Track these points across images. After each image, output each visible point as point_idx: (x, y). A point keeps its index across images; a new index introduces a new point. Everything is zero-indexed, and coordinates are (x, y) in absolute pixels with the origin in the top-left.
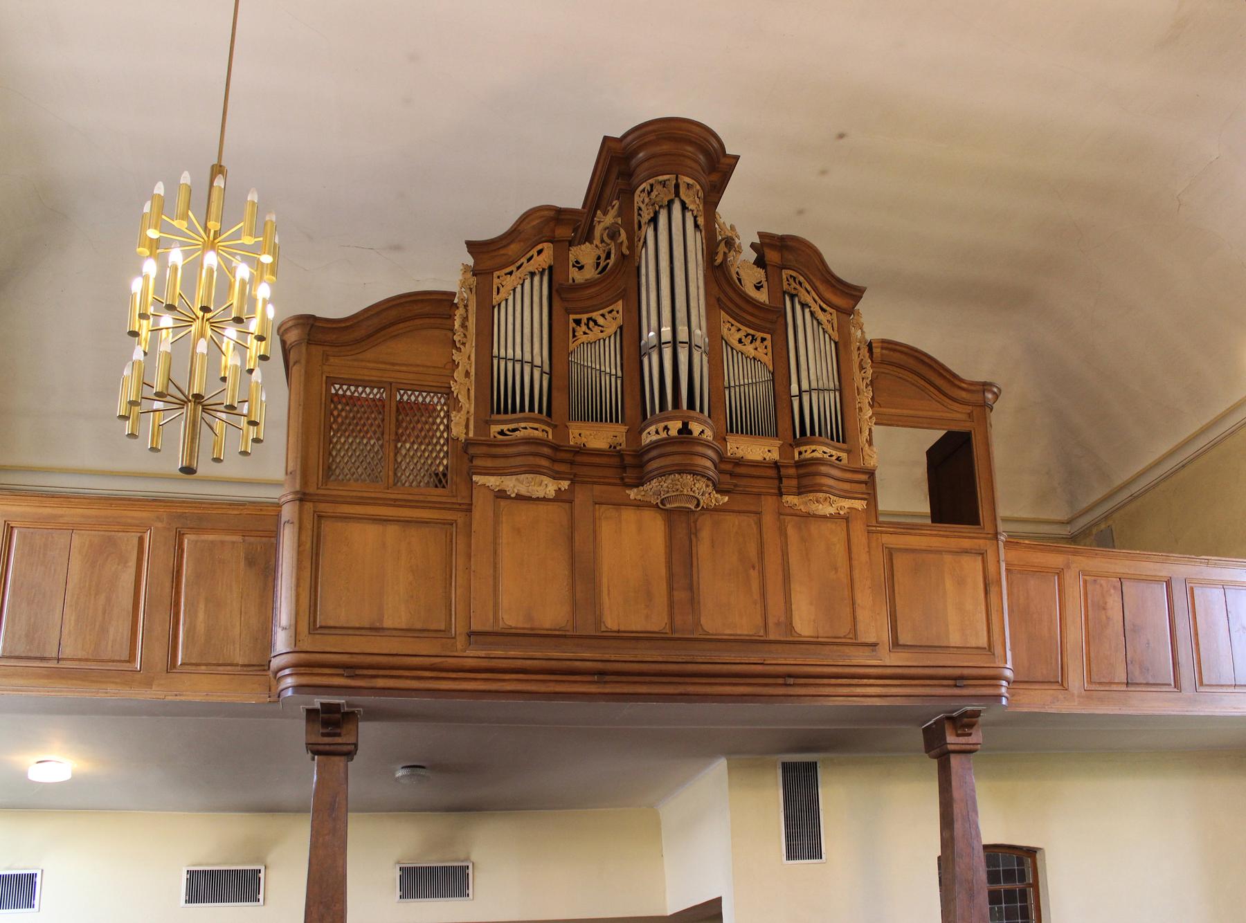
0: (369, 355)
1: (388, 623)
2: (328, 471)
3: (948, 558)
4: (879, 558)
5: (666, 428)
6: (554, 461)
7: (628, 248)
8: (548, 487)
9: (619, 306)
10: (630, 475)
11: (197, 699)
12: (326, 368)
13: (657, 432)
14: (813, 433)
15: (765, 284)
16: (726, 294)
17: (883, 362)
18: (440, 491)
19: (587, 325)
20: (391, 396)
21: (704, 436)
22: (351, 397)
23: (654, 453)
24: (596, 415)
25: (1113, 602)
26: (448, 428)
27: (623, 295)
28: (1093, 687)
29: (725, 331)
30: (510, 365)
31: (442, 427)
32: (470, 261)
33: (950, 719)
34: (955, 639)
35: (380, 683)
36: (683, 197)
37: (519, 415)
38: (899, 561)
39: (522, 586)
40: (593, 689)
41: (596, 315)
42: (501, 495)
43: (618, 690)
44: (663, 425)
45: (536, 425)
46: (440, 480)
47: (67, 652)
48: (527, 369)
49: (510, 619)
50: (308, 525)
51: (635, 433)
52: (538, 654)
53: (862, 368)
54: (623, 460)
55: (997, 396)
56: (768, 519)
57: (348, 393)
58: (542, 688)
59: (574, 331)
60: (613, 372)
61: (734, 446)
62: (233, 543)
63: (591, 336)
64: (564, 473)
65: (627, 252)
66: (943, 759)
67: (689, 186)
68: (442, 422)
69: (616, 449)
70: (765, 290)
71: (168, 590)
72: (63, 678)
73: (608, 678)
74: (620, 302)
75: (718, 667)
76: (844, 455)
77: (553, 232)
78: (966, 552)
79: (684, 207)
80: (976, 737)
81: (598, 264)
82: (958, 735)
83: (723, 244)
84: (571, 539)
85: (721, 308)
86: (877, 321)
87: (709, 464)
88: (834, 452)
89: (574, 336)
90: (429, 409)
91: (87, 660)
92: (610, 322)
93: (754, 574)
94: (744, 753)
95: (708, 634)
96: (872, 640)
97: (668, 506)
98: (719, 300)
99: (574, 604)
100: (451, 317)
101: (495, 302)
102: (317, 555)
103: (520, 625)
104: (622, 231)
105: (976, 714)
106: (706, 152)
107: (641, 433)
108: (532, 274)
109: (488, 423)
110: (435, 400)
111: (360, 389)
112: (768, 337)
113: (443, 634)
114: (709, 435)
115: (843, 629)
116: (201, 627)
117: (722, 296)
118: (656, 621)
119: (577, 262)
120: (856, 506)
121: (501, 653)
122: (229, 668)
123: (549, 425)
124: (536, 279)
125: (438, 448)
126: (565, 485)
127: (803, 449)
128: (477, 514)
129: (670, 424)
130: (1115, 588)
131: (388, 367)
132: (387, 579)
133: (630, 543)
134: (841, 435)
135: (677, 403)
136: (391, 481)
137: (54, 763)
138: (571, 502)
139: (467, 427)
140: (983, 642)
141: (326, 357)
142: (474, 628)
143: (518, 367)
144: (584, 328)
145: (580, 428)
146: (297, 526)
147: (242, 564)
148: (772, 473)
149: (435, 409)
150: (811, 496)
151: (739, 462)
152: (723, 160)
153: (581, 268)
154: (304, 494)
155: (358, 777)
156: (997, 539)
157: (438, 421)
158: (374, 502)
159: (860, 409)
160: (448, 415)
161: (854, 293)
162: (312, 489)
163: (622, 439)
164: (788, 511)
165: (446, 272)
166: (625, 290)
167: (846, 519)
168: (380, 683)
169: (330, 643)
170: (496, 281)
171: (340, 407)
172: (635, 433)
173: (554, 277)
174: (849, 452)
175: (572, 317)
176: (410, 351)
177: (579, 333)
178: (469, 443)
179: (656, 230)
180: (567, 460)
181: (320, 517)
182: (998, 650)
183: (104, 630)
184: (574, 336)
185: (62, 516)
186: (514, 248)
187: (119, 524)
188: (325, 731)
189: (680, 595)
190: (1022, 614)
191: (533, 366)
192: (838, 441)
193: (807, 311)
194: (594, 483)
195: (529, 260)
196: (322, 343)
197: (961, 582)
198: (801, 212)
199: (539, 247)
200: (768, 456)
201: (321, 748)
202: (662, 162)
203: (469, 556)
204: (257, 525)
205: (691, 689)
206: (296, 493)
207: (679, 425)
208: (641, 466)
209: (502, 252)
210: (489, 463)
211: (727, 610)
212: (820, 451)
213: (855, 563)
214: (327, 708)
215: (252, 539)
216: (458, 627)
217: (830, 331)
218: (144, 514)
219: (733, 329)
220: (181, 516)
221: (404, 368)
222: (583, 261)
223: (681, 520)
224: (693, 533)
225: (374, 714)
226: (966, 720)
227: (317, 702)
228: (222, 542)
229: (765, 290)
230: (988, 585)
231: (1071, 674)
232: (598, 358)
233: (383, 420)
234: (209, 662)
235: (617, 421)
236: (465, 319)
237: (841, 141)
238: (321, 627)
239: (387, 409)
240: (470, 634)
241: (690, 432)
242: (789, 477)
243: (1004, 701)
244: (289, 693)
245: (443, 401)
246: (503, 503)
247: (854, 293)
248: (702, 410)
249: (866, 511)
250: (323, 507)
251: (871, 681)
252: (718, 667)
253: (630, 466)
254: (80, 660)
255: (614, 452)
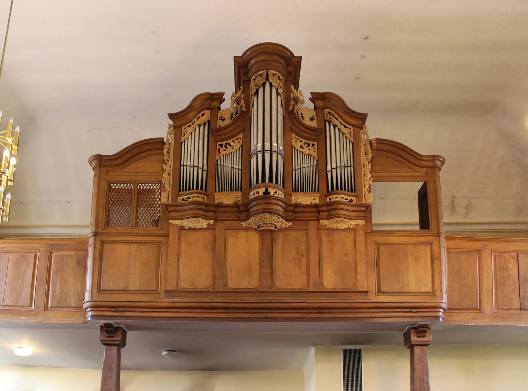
0: (126, 169)
1: (131, 288)
2: (108, 223)
3: (410, 247)
4: (372, 248)
5: (258, 192)
6: (206, 211)
7: (246, 108)
8: (204, 223)
9: (241, 136)
10: (243, 214)
11: (55, 322)
12: (107, 177)
13: (254, 194)
14: (337, 188)
15: (315, 118)
16: (294, 124)
17: (377, 150)
18: (156, 228)
19: (226, 146)
20: (135, 187)
21: (277, 195)
22: (118, 189)
23: (254, 203)
24: (228, 188)
25: (512, 266)
26: (160, 199)
27: (243, 131)
28: (499, 311)
29: (293, 143)
30: (188, 168)
31: (158, 199)
32: (171, 122)
33: (412, 328)
34: (412, 287)
35: (127, 314)
36: (270, 80)
37: (191, 191)
38: (382, 249)
39: (191, 269)
40: (222, 316)
41: (228, 141)
42: (182, 228)
43: (234, 316)
44: (256, 190)
45: (198, 195)
46: (157, 223)
47: (6, 303)
48: (196, 169)
49: (184, 285)
50: (98, 246)
51: (246, 195)
52: (196, 300)
53: (366, 154)
54: (239, 208)
55: (443, 163)
56: (312, 232)
57: (117, 187)
58: (198, 315)
59: (219, 150)
60: (237, 167)
61: (296, 198)
62: (72, 255)
63: (227, 152)
64: (210, 216)
65: (244, 110)
66: (412, 347)
67: (274, 75)
68: (158, 197)
69: (228, 202)
70: (315, 121)
71: (45, 276)
72: (4, 313)
73: (229, 311)
74: (242, 134)
75: (275, 305)
76: (354, 199)
77: (210, 104)
78: (421, 243)
79: (271, 86)
80: (428, 337)
81: (232, 117)
82: (418, 337)
83: (292, 101)
84: (214, 247)
85: (292, 131)
86: (375, 130)
87: (279, 208)
88: (348, 197)
89: (219, 152)
90: (152, 192)
91: (14, 306)
92: (236, 144)
93: (304, 259)
94: (323, 344)
95: (279, 289)
96: (366, 290)
97: (261, 229)
98: (291, 128)
99: (214, 277)
100: (163, 149)
101: (182, 141)
102: (102, 259)
103: (189, 287)
104: (242, 100)
105: (426, 326)
106: (283, 57)
107: (249, 195)
108: (200, 126)
109: (177, 196)
110: (155, 187)
111: (122, 185)
112: (316, 143)
113: (155, 292)
114: (280, 194)
115: (349, 285)
116: (58, 291)
117: (293, 126)
118: (253, 283)
119: (222, 117)
120: (359, 223)
121: (185, 300)
122: (69, 308)
123: (205, 195)
124: (202, 127)
125: (156, 209)
126: (211, 222)
127: (331, 197)
128: (171, 237)
129: (259, 190)
130: (513, 258)
131: (133, 174)
132: (131, 270)
133: (242, 247)
134: (353, 188)
135: (263, 180)
136: (134, 225)
137: (25, 347)
138: (214, 229)
139: (168, 198)
140: (429, 289)
141: (107, 172)
142: (169, 288)
143: (192, 169)
144: (224, 148)
145: (220, 195)
146: (93, 247)
147: (75, 265)
148: (315, 210)
149: (155, 192)
150: (334, 220)
151: (297, 206)
152: (294, 59)
153: (223, 120)
154: (96, 233)
155: (127, 356)
156: (439, 236)
157: (156, 196)
158: (125, 234)
159: (365, 175)
160: (160, 193)
161: (362, 118)
162: (100, 231)
163: (240, 199)
164: (323, 228)
165: (161, 130)
166: (244, 128)
167: (354, 230)
168: (127, 314)
169: (106, 297)
170: (183, 130)
171: (113, 194)
172: (246, 195)
173: (210, 125)
174: (356, 197)
175: (218, 143)
176: (143, 167)
177: (222, 149)
178: (167, 206)
179: (257, 98)
180: (213, 211)
181: (103, 243)
182: (438, 293)
183: (20, 294)
184: (219, 152)
185: (6, 247)
186: (191, 114)
187: (27, 249)
188: (107, 335)
189: (266, 271)
190: (455, 275)
191: (198, 168)
192: (352, 191)
193: (337, 129)
194: (225, 220)
195: (198, 119)
196: (105, 167)
197: (417, 260)
198: (357, 78)
199: (203, 112)
200: (314, 202)
201: (106, 342)
202: (267, 65)
203: (167, 257)
204: (78, 246)
205: (270, 315)
206: (93, 232)
207: (263, 190)
208: (248, 211)
209: (185, 117)
210: (177, 214)
211: (290, 276)
212: (339, 197)
213: (358, 252)
214: (106, 325)
215: (80, 253)
216: (161, 290)
217: (349, 137)
218: (37, 245)
219: (298, 141)
220: (52, 245)
221: (141, 174)
222: (224, 117)
223: (268, 235)
224: (273, 241)
225: (132, 328)
226: (421, 329)
227: (102, 322)
228: (67, 255)
229: (315, 121)
230: (434, 259)
231: (485, 304)
232: (230, 161)
233: (131, 198)
234: (62, 306)
235: (238, 190)
236: (169, 149)
237: (367, 41)
238: (102, 290)
239: (133, 193)
240: (166, 291)
241: (269, 193)
242: (323, 211)
243: (441, 319)
244: (89, 319)
245: (158, 187)
246: (183, 232)
247: (362, 118)
248: (277, 182)
249: (365, 226)
250: (105, 238)
251: (365, 310)
252: (275, 305)
253: (242, 211)
254: (11, 306)
255: (236, 205)
